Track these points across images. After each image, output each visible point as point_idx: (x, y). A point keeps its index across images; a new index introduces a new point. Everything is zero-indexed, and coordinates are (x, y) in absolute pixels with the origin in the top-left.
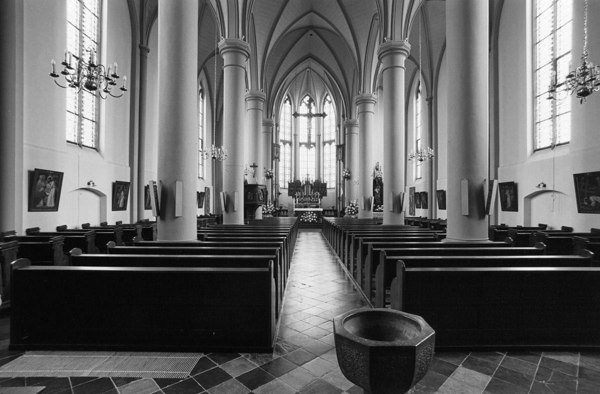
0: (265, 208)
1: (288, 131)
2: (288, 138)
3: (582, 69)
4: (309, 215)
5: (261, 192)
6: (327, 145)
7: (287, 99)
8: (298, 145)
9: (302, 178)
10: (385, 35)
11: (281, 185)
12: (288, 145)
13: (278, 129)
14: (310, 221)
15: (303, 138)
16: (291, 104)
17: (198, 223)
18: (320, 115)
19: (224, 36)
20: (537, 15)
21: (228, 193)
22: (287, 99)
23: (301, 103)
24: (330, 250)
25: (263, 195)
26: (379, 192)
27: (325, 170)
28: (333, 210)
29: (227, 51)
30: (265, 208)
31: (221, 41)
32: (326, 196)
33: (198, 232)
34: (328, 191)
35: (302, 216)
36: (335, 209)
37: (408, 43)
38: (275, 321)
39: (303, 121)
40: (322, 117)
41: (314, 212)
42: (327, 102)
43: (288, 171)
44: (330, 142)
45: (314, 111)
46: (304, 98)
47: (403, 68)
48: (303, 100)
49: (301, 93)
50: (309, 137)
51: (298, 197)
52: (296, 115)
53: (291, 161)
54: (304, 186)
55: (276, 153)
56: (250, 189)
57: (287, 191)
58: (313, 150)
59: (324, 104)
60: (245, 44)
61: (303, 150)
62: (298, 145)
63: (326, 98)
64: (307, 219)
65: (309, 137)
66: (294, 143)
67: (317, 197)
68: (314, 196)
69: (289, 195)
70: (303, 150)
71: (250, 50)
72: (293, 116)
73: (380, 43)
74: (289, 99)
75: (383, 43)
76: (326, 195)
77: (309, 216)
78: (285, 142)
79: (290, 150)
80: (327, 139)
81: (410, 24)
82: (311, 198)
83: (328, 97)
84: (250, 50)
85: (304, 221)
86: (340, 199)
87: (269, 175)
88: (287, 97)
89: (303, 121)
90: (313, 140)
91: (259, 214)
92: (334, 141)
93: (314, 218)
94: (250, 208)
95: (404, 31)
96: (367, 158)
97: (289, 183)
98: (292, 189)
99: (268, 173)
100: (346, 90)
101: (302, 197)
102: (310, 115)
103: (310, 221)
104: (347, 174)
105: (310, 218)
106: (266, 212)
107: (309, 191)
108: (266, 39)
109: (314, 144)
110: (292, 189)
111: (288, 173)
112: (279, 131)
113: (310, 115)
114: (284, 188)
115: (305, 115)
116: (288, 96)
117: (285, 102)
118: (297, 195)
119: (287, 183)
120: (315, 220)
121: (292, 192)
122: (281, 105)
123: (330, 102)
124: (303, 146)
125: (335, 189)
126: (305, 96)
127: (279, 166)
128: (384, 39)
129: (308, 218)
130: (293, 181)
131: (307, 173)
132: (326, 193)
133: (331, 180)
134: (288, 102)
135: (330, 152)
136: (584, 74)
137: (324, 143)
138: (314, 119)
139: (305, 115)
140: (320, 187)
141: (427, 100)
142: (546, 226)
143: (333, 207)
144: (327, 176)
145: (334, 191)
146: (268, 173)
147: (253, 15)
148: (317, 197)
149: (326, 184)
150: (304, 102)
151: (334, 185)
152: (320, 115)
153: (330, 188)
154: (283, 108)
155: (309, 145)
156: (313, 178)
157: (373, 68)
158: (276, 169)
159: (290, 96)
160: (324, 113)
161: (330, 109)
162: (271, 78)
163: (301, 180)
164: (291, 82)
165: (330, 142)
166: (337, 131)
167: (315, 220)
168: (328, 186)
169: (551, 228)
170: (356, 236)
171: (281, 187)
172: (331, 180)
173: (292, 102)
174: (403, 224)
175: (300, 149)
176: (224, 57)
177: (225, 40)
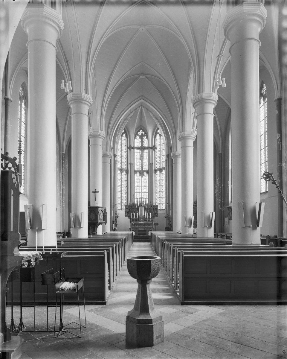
1: (124, 160)
5: (101, 212)
6: (158, 172)
8: (133, 172)
9: (136, 201)
11: (119, 207)
15: (137, 167)
16: (127, 137)
17: (197, 225)
20: (263, 106)
22: (123, 133)
25: (103, 215)
32: (158, 216)
33: (57, 241)
34: (159, 212)
39: (137, 153)
42: (158, 136)
44: (161, 170)
45: (146, 144)
47: (212, 114)
50: (142, 167)
52: (130, 148)
54: (138, 207)
56: (93, 211)
58: (146, 177)
59: (155, 137)
61: (137, 177)
62: (133, 172)
63: (157, 131)
65: (142, 167)
66: (129, 171)
69: (125, 216)
70: (137, 177)
71: (92, 101)
72: (128, 149)
76: (157, 215)
78: (121, 170)
80: (158, 167)
83: (159, 131)
84: (91, 101)
88: (123, 131)
89: (137, 153)
90: (146, 167)
91: (100, 231)
94: (93, 225)
96: (187, 184)
97: (126, 206)
98: (128, 210)
110: (128, 210)
113: (142, 148)
114: (122, 210)
115: (138, 148)
116: (124, 130)
117: (122, 136)
119: (124, 206)
121: (128, 213)
123: (160, 135)
124: (138, 173)
127: (117, 190)
130: (129, 204)
133: (161, 203)
134: (124, 135)
135: (161, 178)
137: (156, 171)
139: (138, 148)
140: (152, 209)
145: (164, 212)
149: (157, 206)
151: (164, 207)
155: (141, 173)
161: (161, 142)
163: (136, 203)
170: (179, 250)
172: (161, 203)
173: (128, 134)
174: (259, 242)
175: (135, 176)
176: (71, 106)
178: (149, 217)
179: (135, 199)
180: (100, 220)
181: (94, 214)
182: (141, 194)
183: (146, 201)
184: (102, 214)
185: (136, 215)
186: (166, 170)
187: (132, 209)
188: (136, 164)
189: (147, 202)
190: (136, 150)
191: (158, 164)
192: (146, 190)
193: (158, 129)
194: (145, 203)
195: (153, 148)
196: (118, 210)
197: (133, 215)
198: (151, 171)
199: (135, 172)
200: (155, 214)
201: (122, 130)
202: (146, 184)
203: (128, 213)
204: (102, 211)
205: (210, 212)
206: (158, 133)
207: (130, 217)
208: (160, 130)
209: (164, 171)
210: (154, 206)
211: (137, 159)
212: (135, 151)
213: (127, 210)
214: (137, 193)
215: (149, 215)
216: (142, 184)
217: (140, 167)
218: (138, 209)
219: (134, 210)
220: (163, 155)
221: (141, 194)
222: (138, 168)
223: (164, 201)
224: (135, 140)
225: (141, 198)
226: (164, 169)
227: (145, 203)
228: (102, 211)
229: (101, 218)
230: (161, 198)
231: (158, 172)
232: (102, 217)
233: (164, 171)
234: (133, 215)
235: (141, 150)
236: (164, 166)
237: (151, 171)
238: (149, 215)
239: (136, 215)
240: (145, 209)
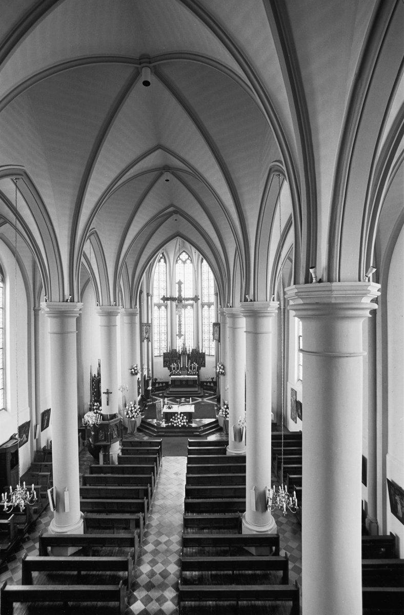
0: (129, 412)
4: (178, 418)
6: (206, 307)
7: (161, 258)
9: (179, 347)
11: (156, 353)
14: (180, 426)
16: (165, 262)
21: (59, 490)
22: (161, 258)
23: (177, 261)
27: (204, 335)
28: (213, 382)
30: (129, 412)
34: (207, 358)
35: (171, 420)
36: (214, 380)
38: (251, 93)
43: (163, 337)
46: (180, 254)
48: (179, 257)
49: (176, 251)
51: (174, 368)
53: (167, 325)
55: (146, 333)
64: (176, 423)
67: (194, 368)
68: (191, 368)
77: (179, 420)
79: (165, 313)
80: (206, 300)
82: (188, 370)
85: (173, 425)
87: (134, 372)
88: (161, 256)
92: (213, 304)
93: (184, 422)
95: (271, 288)
99: (133, 370)
100: (218, 270)
101: (178, 368)
103: (180, 426)
104: (221, 370)
105: (180, 423)
106: (131, 416)
107: (184, 362)
108: (120, 239)
110: (167, 359)
111: (163, 331)
116: (163, 254)
118: (172, 366)
120: (185, 424)
122: (155, 264)
126: (182, 252)
129: (178, 422)
130: (169, 351)
134: (162, 260)
137: (203, 306)
143: (213, 379)
144: (206, 342)
146: (133, 370)
148: (194, 368)
150: (180, 259)
153: (209, 355)
154: (157, 268)
156: (190, 346)
159: (165, 254)
162: (133, 263)
165: (209, 305)
167: (185, 424)
218: (180, 358)
219: (175, 358)
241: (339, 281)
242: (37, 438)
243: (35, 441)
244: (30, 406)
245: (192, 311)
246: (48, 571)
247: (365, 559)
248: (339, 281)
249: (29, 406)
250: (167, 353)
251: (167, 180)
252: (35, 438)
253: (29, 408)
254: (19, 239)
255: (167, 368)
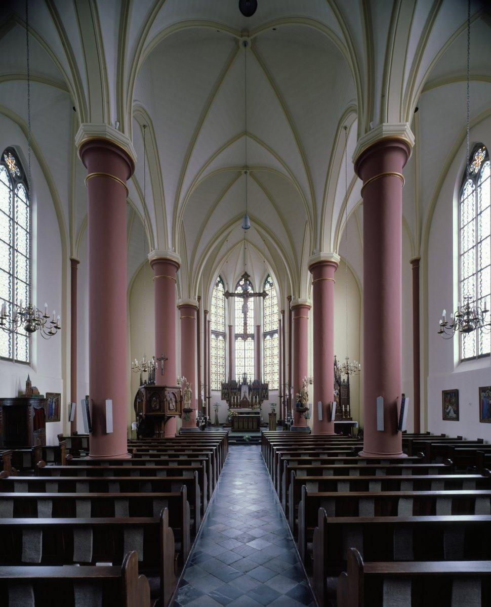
2: (221, 329)
3: (467, 309)
5: (172, 396)
6: (268, 337)
10: (371, 118)
12: (221, 338)
13: (207, 318)
15: (239, 330)
18: (259, 295)
19: (153, 246)
22: (219, 282)
24: (262, 459)
25: (176, 402)
26: (338, 394)
29: (156, 263)
31: (151, 252)
34: (270, 393)
37: (337, 255)
39: (238, 302)
40: (262, 298)
41: (195, 477)
44: (271, 333)
52: (228, 295)
54: (240, 386)
57: (219, 394)
58: (250, 344)
60: (174, 255)
61: (239, 344)
73: (359, 135)
74: (221, 281)
75: (313, 255)
78: (217, 334)
80: (268, 329)
81: (341, 226)
83: (270, 279)
86: (286, 402)
88: (218, 279)
90: (251, 330)
98: (226, 391)
102: (245, 295)
109: (252, 336)
110: (226, 391)
112: (209, 322)
113: (245, 295)
116: (220, 277)
117: (217, 285)
121: (226, 394)
123: (271, 285)
125: (279, 391)
128: (313, 250)
130: (227, 382)
131: (244, 369)
132: (267, 396)
133: (272, 379)
134: (220, 285)
136: (468, 313)
137: (265, 335)
138: (252, 299)
140: (259, 389)
141: (411, 263)
142: (445, 435)
145: (277, 393)
147: (183, 223)
151: (276, 386)
152: (259, 295)
153: (272, 390)
155: (245, 336)
157: (333, 220)
158: (131, 110)
160: (264, 292)
163: (237, 380)
164: (223, 258)
166: (280, 320)
168: (270, 387)
169: (465, 439)
171: (214, 388)
172: (272, 379)
177: (156, 251)
178: (256, 401)
179: (236, 376)
180: (169, 409)
181: (158, 400)
182: (245, 368)
183: (251, 378)
184: (174, 399)
185: (237, 398)
186: (279, 333)
187: (232, 389)
188: (238, 326)
189: (253, 380)
190: (237, 299)
191: (268, 325)
192: (252, 362)
193: (268, 276)
194: (250, 381)
195: (264, 295)
196: (212, 390)
197: (234, 398)
198: (258, 337)
199: (237, 336)
200: (264, 396)
201: (217, 279)
202: (251, 354)
203: (226, 394)
204: (173, 393)
205: (396, 398)
206: (269, 282)
207: (229, 401)
208: (272, 279)
209: (276, 336)
210: (262, 384)
211: (238, 311)
212: (236, 300)
213: (224, 390)
214: (239, 367)
215: (256, 398)
216: (246, 355)
217: (243, 331)
218: (240, 389)
219: (235, 391)
220: (275, 312)
221: (245, 368)
222: (240, 331)
223: (276, 377)
224: (236, 341)
225: (245, 374)
226: (275, 332)
227: (250, 381)
228: (173, 393)
229: (172, 407)
230: (273, 373)
231: (268, 337)
232: (174, 404)
233: (276, 336)
234: (234, 398)
235: (244, 297)
236: (276, 327)
237: (258, 337)
238: (256, 398)
239: (237, 398)
240: (250, 389)
241: (90, 122)
242: (72, 419)
243: (69, 424)
244: (64, 378)
245: (253, 343)
246: (146, 393)
247: (358, 514)
248: (90, 122)
249: (63, 379)
250: (225, 383)
251: (274, 29)
252: (69, 421)
253: (62, 381)
254: (465, 274)
255: (225, 401)
